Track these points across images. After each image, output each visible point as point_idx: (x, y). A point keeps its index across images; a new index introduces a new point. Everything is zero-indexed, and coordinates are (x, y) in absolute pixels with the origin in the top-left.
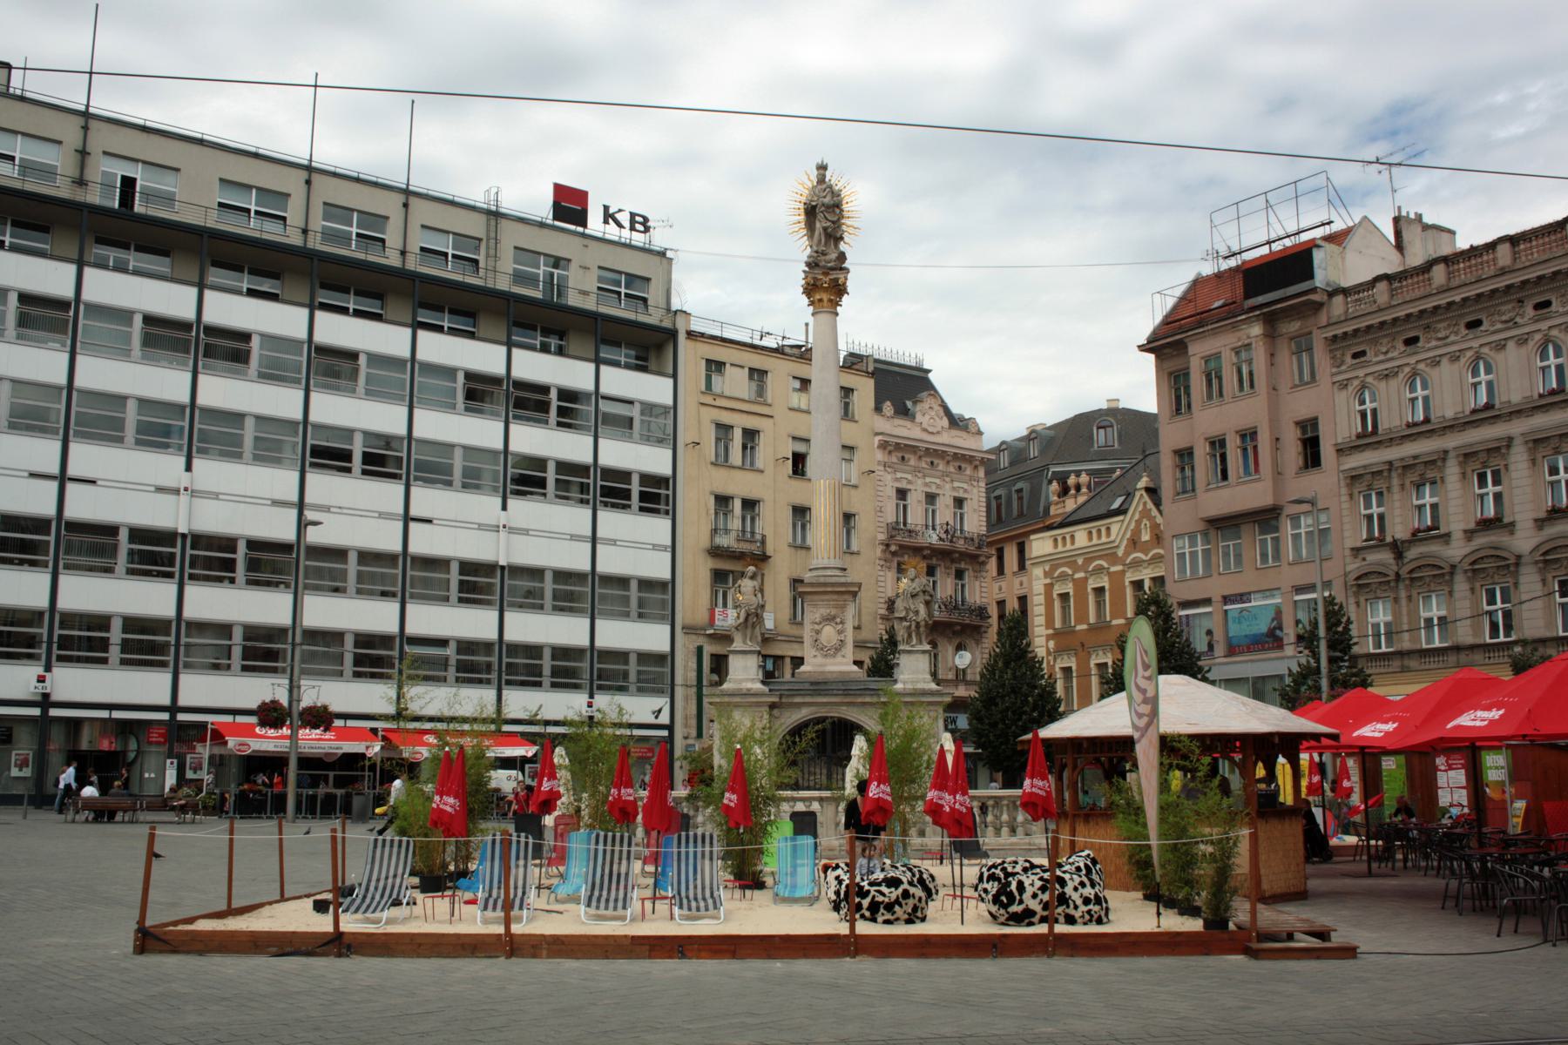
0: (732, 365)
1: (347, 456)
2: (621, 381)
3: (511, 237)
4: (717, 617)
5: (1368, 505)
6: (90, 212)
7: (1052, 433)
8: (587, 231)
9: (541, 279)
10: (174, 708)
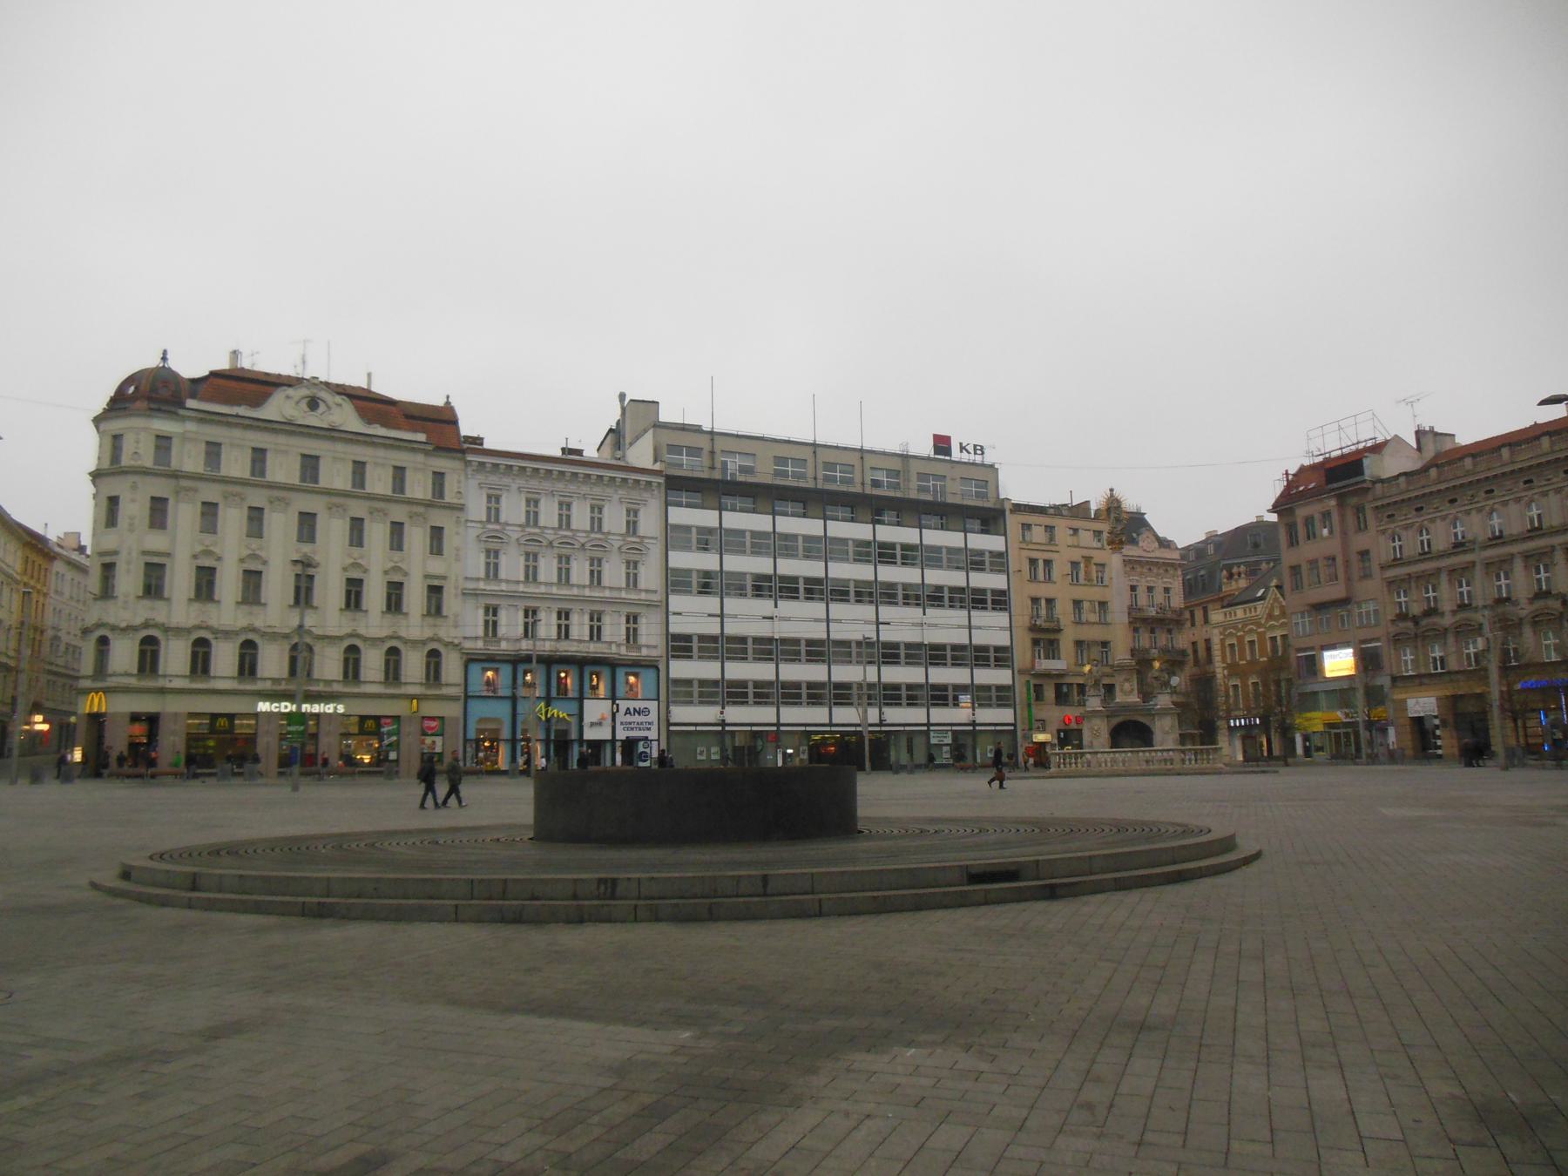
3: (915, 468)
5: (1399, 597)
7: (1220, 539)
8: (953, 459)
10: (778, 724)
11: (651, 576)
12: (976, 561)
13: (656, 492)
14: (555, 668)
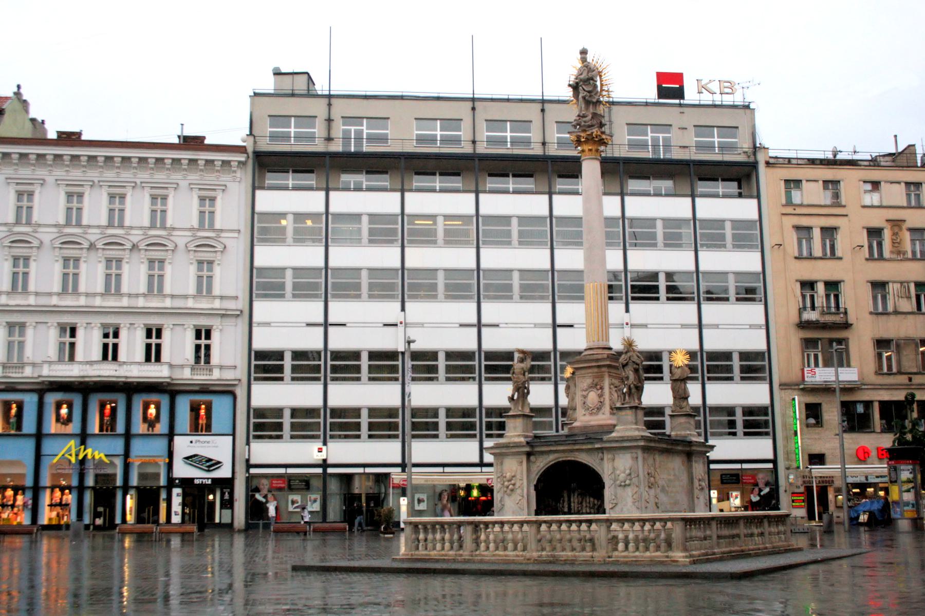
0: (886, 182)
4: (806, 375)
6: (405, 158)
8: (685, 102)
9: (650, 144)
13: (238, 174)
14: (138, 402)
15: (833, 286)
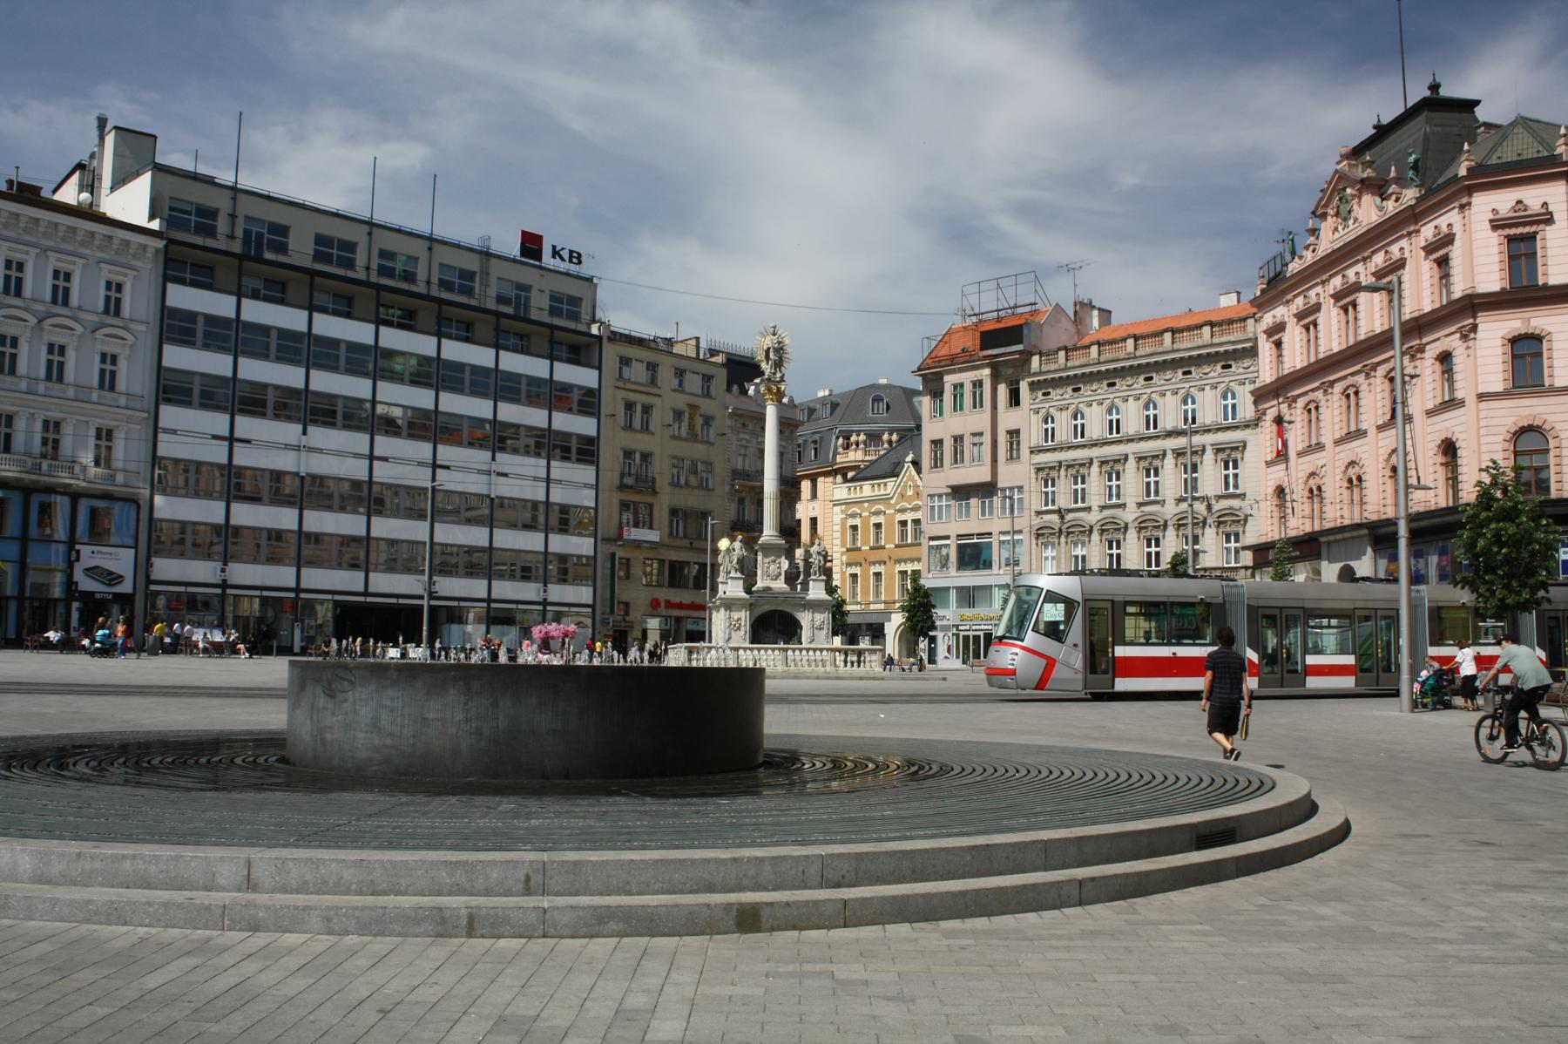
0: (637, 360)
1: (189, 392)
2: (568, 373)
10: (298, 590)
11: (134, 377)
12: (556, 396)
15: (646, 457)
